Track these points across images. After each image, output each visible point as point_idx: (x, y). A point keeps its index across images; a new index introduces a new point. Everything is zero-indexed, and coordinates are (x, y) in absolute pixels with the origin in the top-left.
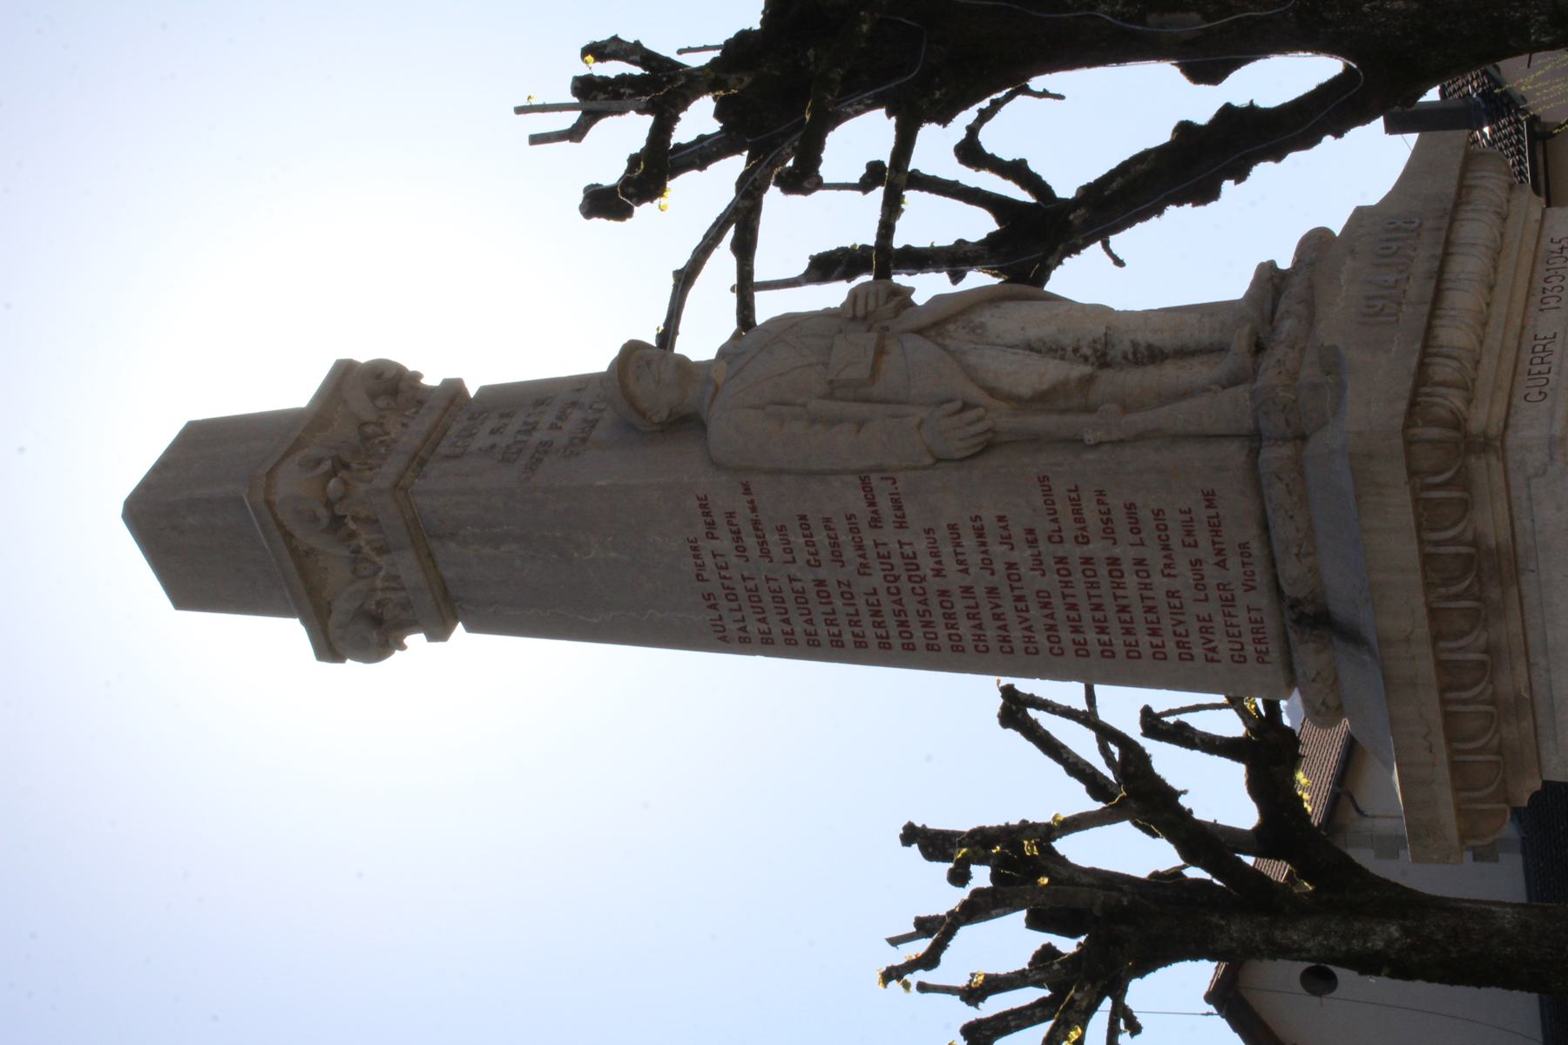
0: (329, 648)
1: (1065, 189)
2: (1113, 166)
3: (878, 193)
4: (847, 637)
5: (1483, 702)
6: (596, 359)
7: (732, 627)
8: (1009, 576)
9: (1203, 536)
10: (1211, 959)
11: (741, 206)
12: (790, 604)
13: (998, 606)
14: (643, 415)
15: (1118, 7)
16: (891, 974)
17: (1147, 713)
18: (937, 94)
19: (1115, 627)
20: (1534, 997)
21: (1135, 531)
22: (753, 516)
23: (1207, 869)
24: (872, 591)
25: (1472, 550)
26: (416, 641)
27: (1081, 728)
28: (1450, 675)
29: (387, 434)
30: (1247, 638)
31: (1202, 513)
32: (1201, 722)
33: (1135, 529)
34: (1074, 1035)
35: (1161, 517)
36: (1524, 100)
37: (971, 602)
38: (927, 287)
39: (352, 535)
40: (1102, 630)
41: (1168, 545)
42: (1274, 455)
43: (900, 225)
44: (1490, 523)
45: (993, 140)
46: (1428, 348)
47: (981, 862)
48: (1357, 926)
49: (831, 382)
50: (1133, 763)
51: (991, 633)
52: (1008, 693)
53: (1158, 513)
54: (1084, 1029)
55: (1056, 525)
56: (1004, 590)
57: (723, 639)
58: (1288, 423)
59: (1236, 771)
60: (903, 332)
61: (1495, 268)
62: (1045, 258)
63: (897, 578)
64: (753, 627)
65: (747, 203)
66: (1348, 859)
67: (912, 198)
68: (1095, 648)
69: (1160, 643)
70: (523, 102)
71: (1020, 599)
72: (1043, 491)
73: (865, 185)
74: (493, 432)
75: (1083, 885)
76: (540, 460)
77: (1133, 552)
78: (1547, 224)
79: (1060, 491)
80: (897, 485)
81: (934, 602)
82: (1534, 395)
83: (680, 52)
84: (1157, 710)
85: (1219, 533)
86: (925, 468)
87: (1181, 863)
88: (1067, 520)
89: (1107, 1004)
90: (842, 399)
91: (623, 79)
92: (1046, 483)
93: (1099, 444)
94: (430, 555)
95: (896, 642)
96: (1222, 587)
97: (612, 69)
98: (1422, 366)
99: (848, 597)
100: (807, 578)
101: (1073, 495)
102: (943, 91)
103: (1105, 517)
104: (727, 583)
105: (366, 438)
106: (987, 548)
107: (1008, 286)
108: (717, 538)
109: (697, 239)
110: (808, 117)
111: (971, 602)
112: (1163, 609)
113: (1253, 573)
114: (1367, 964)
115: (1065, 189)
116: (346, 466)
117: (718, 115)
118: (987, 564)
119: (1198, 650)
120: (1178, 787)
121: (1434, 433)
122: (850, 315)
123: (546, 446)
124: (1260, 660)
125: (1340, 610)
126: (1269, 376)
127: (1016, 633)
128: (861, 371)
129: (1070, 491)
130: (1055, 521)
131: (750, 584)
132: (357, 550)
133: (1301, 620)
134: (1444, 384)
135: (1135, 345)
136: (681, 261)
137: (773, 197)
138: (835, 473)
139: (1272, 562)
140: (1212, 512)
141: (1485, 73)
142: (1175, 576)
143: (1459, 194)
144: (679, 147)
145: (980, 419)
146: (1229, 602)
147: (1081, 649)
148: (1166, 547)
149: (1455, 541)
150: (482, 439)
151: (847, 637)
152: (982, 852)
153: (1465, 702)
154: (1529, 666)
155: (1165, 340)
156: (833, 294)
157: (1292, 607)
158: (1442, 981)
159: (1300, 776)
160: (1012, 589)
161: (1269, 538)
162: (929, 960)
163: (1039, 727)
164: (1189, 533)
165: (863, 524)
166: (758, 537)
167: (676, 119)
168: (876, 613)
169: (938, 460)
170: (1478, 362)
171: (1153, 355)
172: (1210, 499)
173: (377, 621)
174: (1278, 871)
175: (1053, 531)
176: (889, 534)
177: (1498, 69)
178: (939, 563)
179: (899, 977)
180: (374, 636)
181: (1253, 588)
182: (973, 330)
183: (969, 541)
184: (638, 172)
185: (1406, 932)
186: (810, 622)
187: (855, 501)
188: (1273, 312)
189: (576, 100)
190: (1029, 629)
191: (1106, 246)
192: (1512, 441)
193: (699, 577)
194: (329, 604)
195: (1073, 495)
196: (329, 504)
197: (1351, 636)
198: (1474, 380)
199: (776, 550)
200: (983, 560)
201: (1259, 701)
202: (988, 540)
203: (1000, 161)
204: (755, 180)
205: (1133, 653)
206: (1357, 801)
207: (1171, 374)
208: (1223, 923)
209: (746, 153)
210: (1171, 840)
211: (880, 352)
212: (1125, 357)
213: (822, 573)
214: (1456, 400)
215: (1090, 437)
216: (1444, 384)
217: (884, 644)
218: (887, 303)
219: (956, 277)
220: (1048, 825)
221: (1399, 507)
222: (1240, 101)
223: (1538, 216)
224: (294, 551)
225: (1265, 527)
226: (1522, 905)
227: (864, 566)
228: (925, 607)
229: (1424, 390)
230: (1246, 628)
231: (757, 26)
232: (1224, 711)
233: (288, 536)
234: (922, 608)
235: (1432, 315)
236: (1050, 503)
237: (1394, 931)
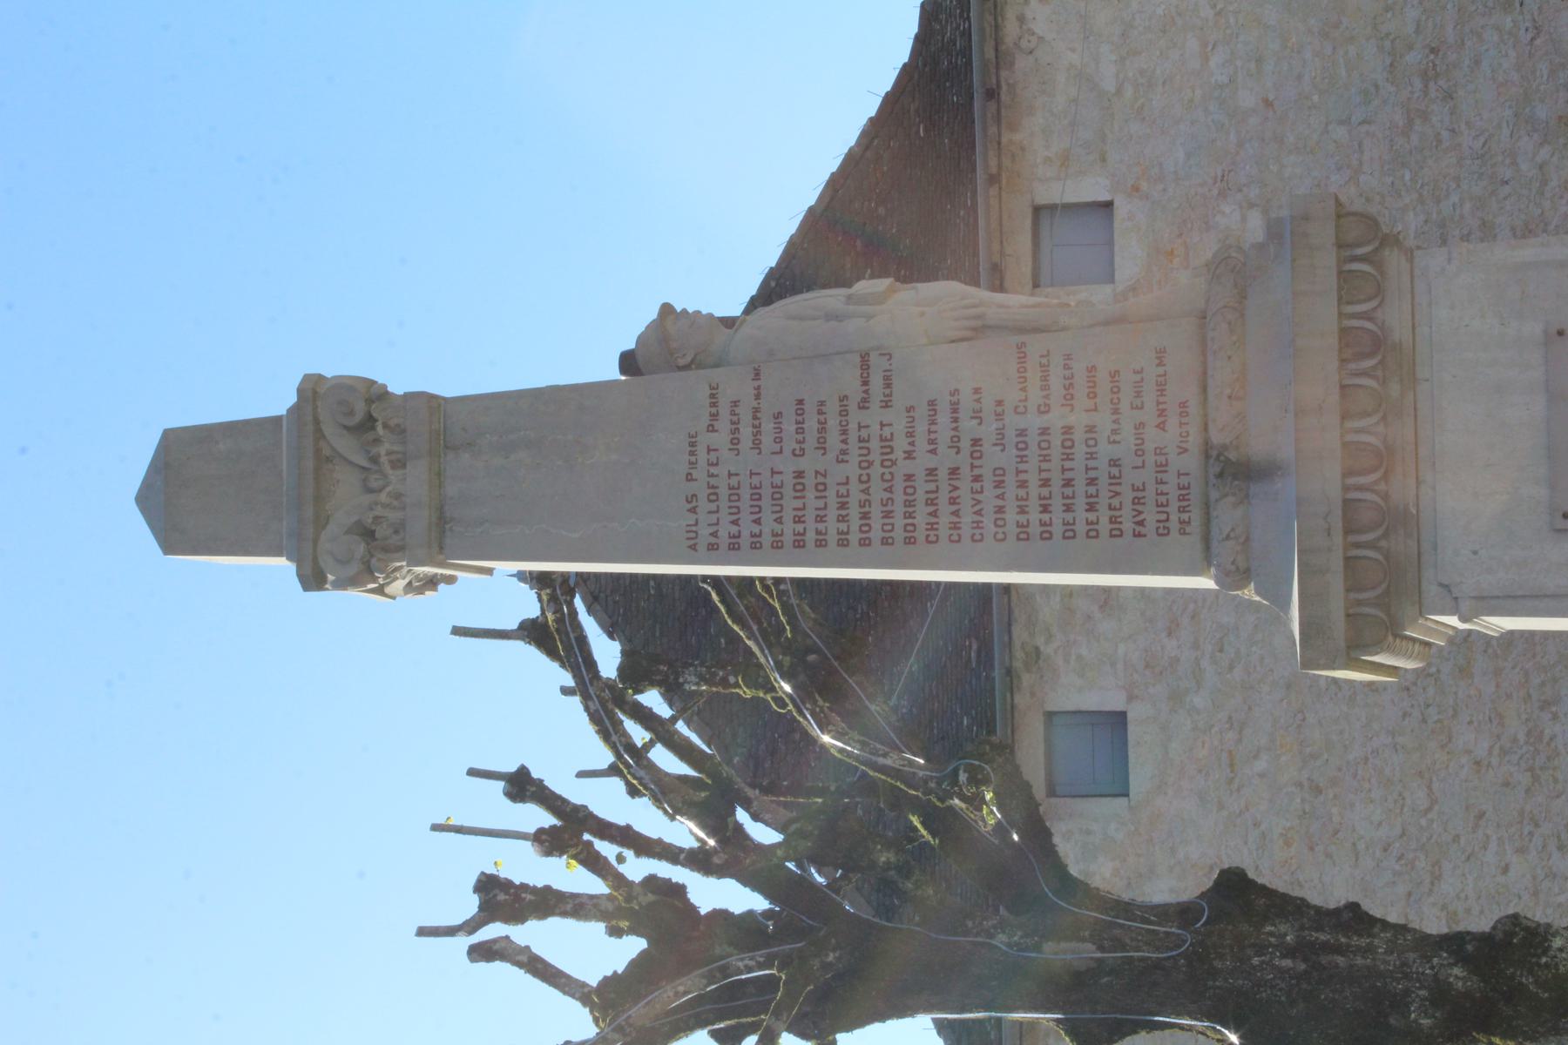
11: (609, 1037)
13: (956, 488)
15: (1016, 938)
21: (1091, 395)
24: (845, 481)
33: (1092, 395)
35: (1117, 378)
41: (1118, 409)
44: (1395, 317)
55: (1024, 394)
56: (966, 472)
57: (693, 547)
63: (870, 464)
69: (1095, 520)
70: (441, 821)
71: (977, 479)
72: (1019, 358)
80: (891, 362)
81: (899, 485)
85: (1164, 393)
92: (1023, 350)
96: (1159, 451)
100: (787, 466)
101: (1044, 361)
102: (837, 955)
103: (1067, 382)
106: (959, 424)
108: (717, 431)
112: (1104, 481)
118: (955, 443)
124: (1182, 531)
129: (1042, 356)
130: (1024, 389)
140: (1161, 370)
142: (1119, 442)
148: (1116, 411)
154: (1418, 483)
161: (1206, 399)
165: (852, 407)
166: (754, 426)
168: (843, 506)
175: (1020, 401)
178: (912, 444)
181: (1186, 450)
183: (944, 419)
193: (689, 478)
195: (1044, 361)
199: (767, 440)
200: (952, 437)
204: (630, 1017)
213: (804, 464)
225: (1204, 389)
228: (889, 495)
230: (1174, 494)
233: (319, 434)
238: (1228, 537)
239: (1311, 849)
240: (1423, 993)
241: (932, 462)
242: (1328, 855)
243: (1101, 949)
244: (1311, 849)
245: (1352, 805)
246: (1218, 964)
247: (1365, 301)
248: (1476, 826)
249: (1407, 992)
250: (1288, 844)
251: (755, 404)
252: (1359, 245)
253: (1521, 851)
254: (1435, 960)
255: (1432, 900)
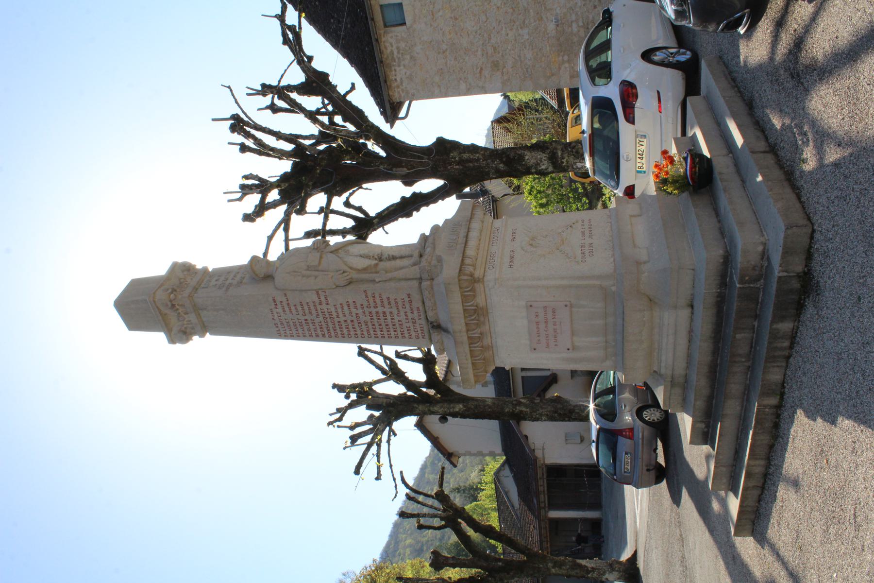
0: (172, 340)
1: (372, 214)
2: (385, 208)
3: (323, 215)
4: (314, 334)
5: (480, 347)
6: (244, 260)
7: (282, 332)
8: (356, 317)
9: (408, 306)
10: (415, 416)
12: (298, 326)
13: (354, 325)
14: (257, 275)
16: (330, 423)
17: (396, 352)
18: (338, 189)
19: (385, 330)
20: (497, 422)
22: (287, 302)
23: (413, 392)
25: (476, 308)
26: (196, 338)
27: (379, 356)
28: (472, 341)
29: (187, 281)
30: (420, 332)
31: (407, 299)
32: (410, 354)
33: (390, 304)
34: (379, 437)
36: (491, 191)
37: (347, 324)
38: (333, 240)
39: (177, 309)
40: (381, 331)
42: (425, 284)
43: (328, 223)
44: (480, 300)
45: (352, 201)
46: (464, 257)
47: (353, 393)
48: (452, 405)
49: (308, 266)
50: (393, 366)
51: (352, 333)
52: (360, 348)
53: (395, 300)
54: (381, 436)
57: (280, 335)
58: (429, 276)
59: (420, 367)
60: (327, 252)
61: (481, 235)
62: (367, 232)
63: (327, 318)
64: (288, 332)
65: (287, 218)
66: (449, 388)
67: (331, 216)
68: (380, 336)
71: (359, 323)
73: (319, 213)
74: (216, 281)
75: (380, 398)
76: (229, 288)
77: (389, 310)
78: (494, 224)
79: (369, 293)
81: (337, 324)
82: (491, 268)
83: (269, 177)
84: (399, 351)
86: (334, 288)
87: (406, 391)
88: (371, 300)
89: (388, 428)
90: (310, 271)
91: (253, 185)
93: (380, 282)
94: (199, 314)
95: (327, 335)
96: (413, 319)
97: (250, 182)
98: (463, 260)
99: (314, 324)
100: (303, 318)
101: (373, 295)
104: (281, 321)
105: (181, 283)
107: (357, 240)
109: (274, 228)
110: (303, 195)
111: (347, 324)
112: (397, 325)
113: (421, 315)
114: (455, 415)
115: (372, 214)
116: (175, 291)
117: (279, 194)
118: (351, 314)
119: (407, 335)
120: (405, 371)
121: (466, 278)
122: (313, 248)
123: (231, 284)
125: (443, 325)
126: (424, 262)
127: (359, 332)
128: (317, 263)
130: (368, 302)
131: (287, 321)
132: (179, 313)
133: (433, 327)
134: (468, 265)
135: (389, 255)
136: (269, 233)
137: (294, 216)
138: (309, 290)
139: (426, 312)
141: (481, 184)
143: (471, 216)
144: (268, 203)
145: (348, 275)
146: (414, 322)
147: (376, 336)
149: (471, 305)
150: (213, 282)
151: (314, 334)
152: (353, 390)
153: (475, 347)
155: (396, 254)
156: (309, 242)
157: (431, 324)
158: (473, 418)
159: (437, 367)
160: (357, 320)
161: (424, 306)
162: (340, 419)
163: (368, 356)
164: (404, 305)
165: (317, 304)
167: (267, 195)
169: (337, 286)
170: (477, 259)
171: (394, 258)
172: (409, 296)
173: (185, 333)
174: (432, 392)
176: (324, 307)
177: (483, 183)
179: (332, 424)
180: (184, 337)
181: (421, 319)
182: (346, 252)
183: (346, 308)
184: (257, 209)
185: (464, 406)
186: (303, 330)
187: (315, 298)
188: (425, 246)
189: (240, 190)
190: (362, 331)
191: (383, 228)
192: (485, 279)
193: (273, 319)
194: (172, 328)
195: (373, 295)
196: (171, 301)
197: (446, 331)
198: (476, 264)
199: (294, 311)
201: (426, 349)
202: (351, 307)
203: (355, 206)
205: (390, 337)
206: (453, 373)
207: (399, 263)
208: (417, 406)
209: (287, 204)
210: (403, 385)
211: (321, 257)
212: (386, 258)
213: (306, 317)
214: (471, 269)
215: (377, 280)
216: (468, 265)
217: (324, 336)
218: (323, 244)
219: (344, 237)
220: (371, 382)
221: (457, 297)
222: (417, 191)
223: (491, 221)
224: (161, 314)
225: (424, 303)
226: (493, 398)
227: (318, 315)
229: (463, 266)
230: (419, 329)
231: (289, 171)
232: (417, 351)
233: (159, 310)
234: (333, 326)
235: (465, 247)
236: (367, 297)
237: (461, 406)
238: (437, 343)
239: (457, 34)
240: (493, 171)
241: (345, 319)
242: (461, 36)
243: (409, 169)
244: (457, 34)
245: (466, 22)
246: (439, 169)
247: (472, 301)
248: (499, 25)
249: (489, 171)
250: (450, 34)
251: (287, 302)
252: (468, 288)
253: (511, 30)
254: (496, 162)
255: (489, 44)
